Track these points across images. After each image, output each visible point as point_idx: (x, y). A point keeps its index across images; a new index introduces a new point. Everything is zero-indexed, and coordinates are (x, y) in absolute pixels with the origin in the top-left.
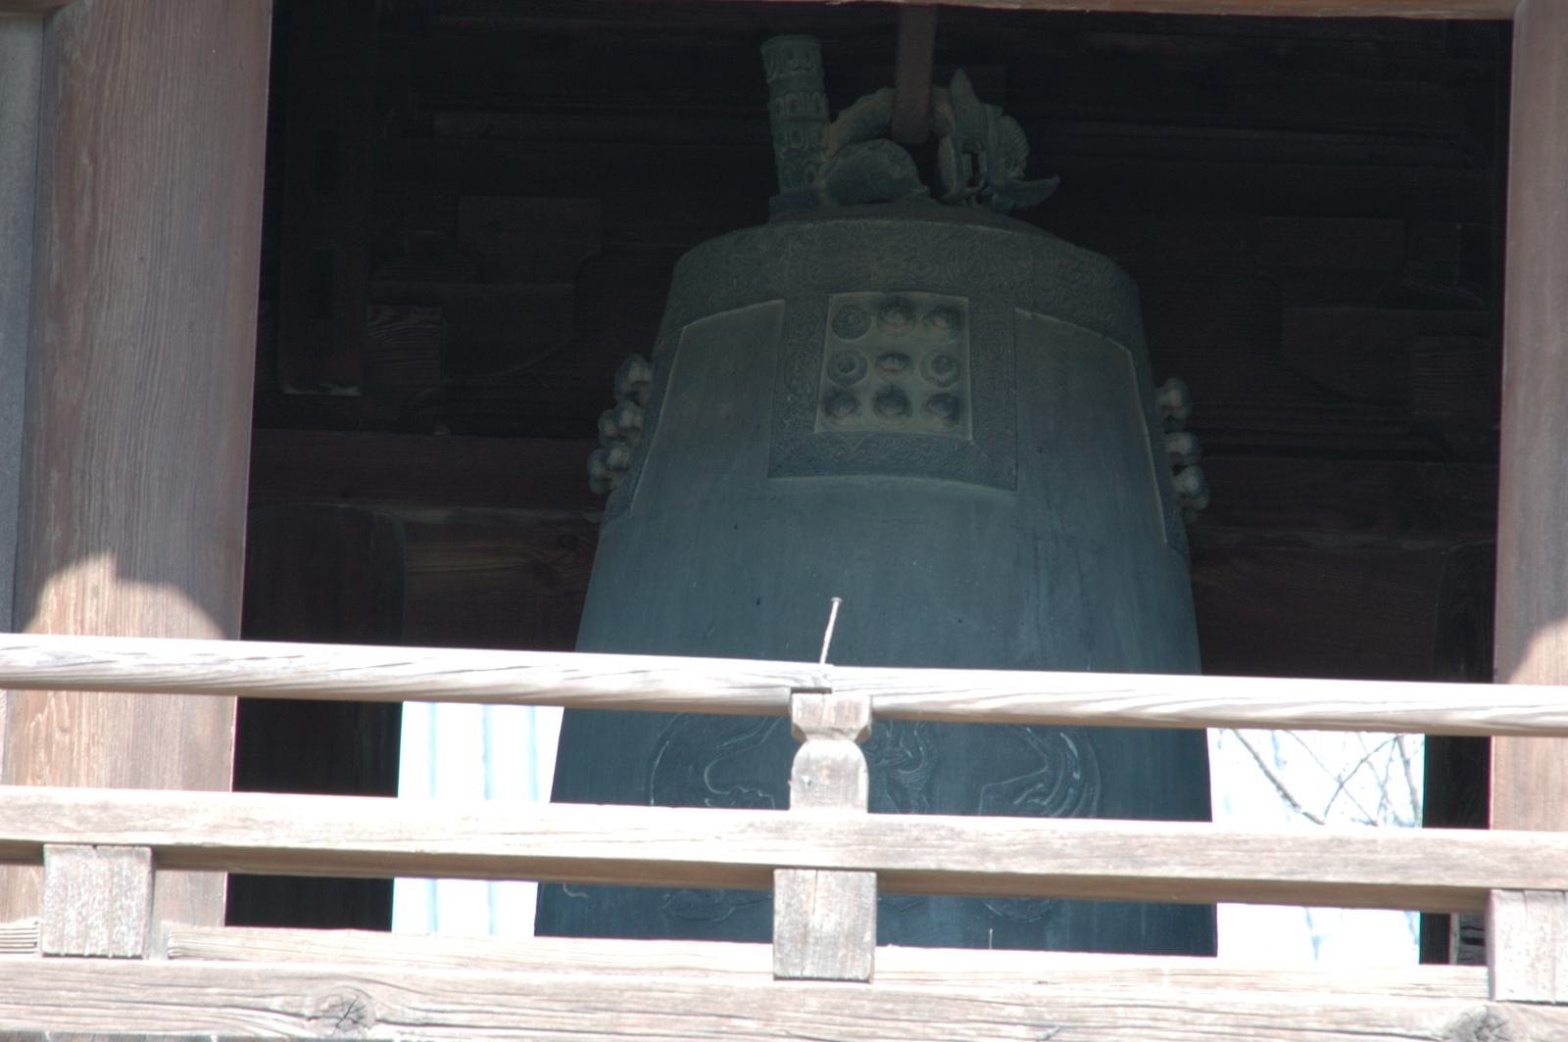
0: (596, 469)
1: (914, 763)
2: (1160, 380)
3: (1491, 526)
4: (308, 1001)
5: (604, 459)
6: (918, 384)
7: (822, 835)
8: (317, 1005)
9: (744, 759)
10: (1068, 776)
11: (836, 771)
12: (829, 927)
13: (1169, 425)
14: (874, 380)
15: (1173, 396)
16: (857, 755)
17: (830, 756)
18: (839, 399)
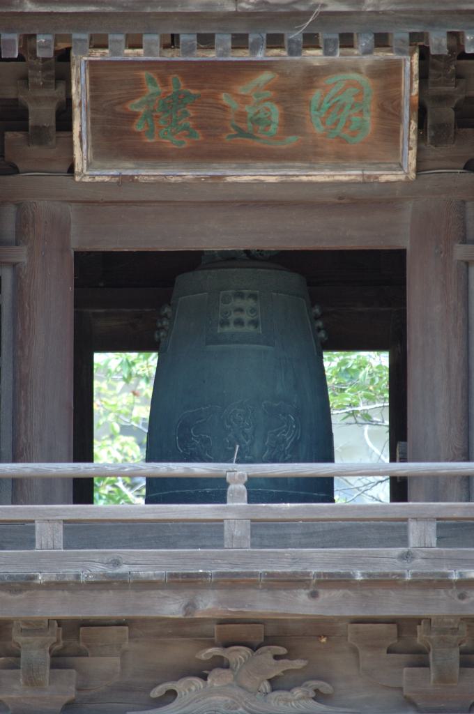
0: (156, 336)
1: (260, 491)
2: (313, 306)
3: (405, 304)
4: (106, 559)
5: (159, 334)
6: (246, 317)
7: (236, 509)
8: (108, 559)
9: (214, 491)
10: (292, 426)
11: (240, 493)
12: (239, 534)
13: (316, 318)
14: (233, 316)
15: (317, 310)
16: (243, 488)
17: (237, 488)
18: (225, 323)
